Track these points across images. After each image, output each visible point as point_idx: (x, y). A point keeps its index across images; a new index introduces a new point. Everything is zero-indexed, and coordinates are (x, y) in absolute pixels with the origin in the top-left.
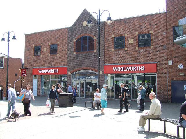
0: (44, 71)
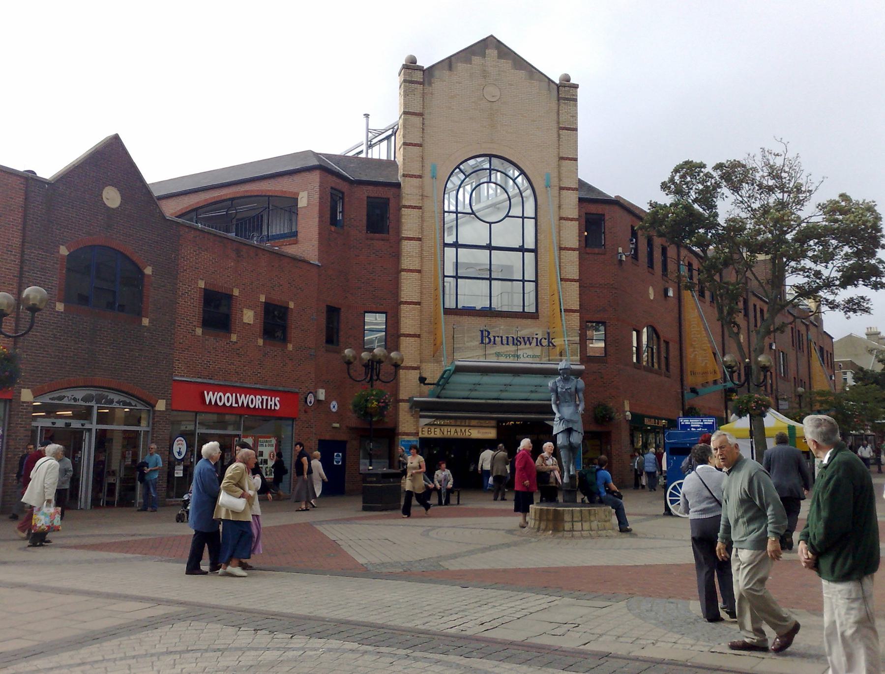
0: (227, 399)
